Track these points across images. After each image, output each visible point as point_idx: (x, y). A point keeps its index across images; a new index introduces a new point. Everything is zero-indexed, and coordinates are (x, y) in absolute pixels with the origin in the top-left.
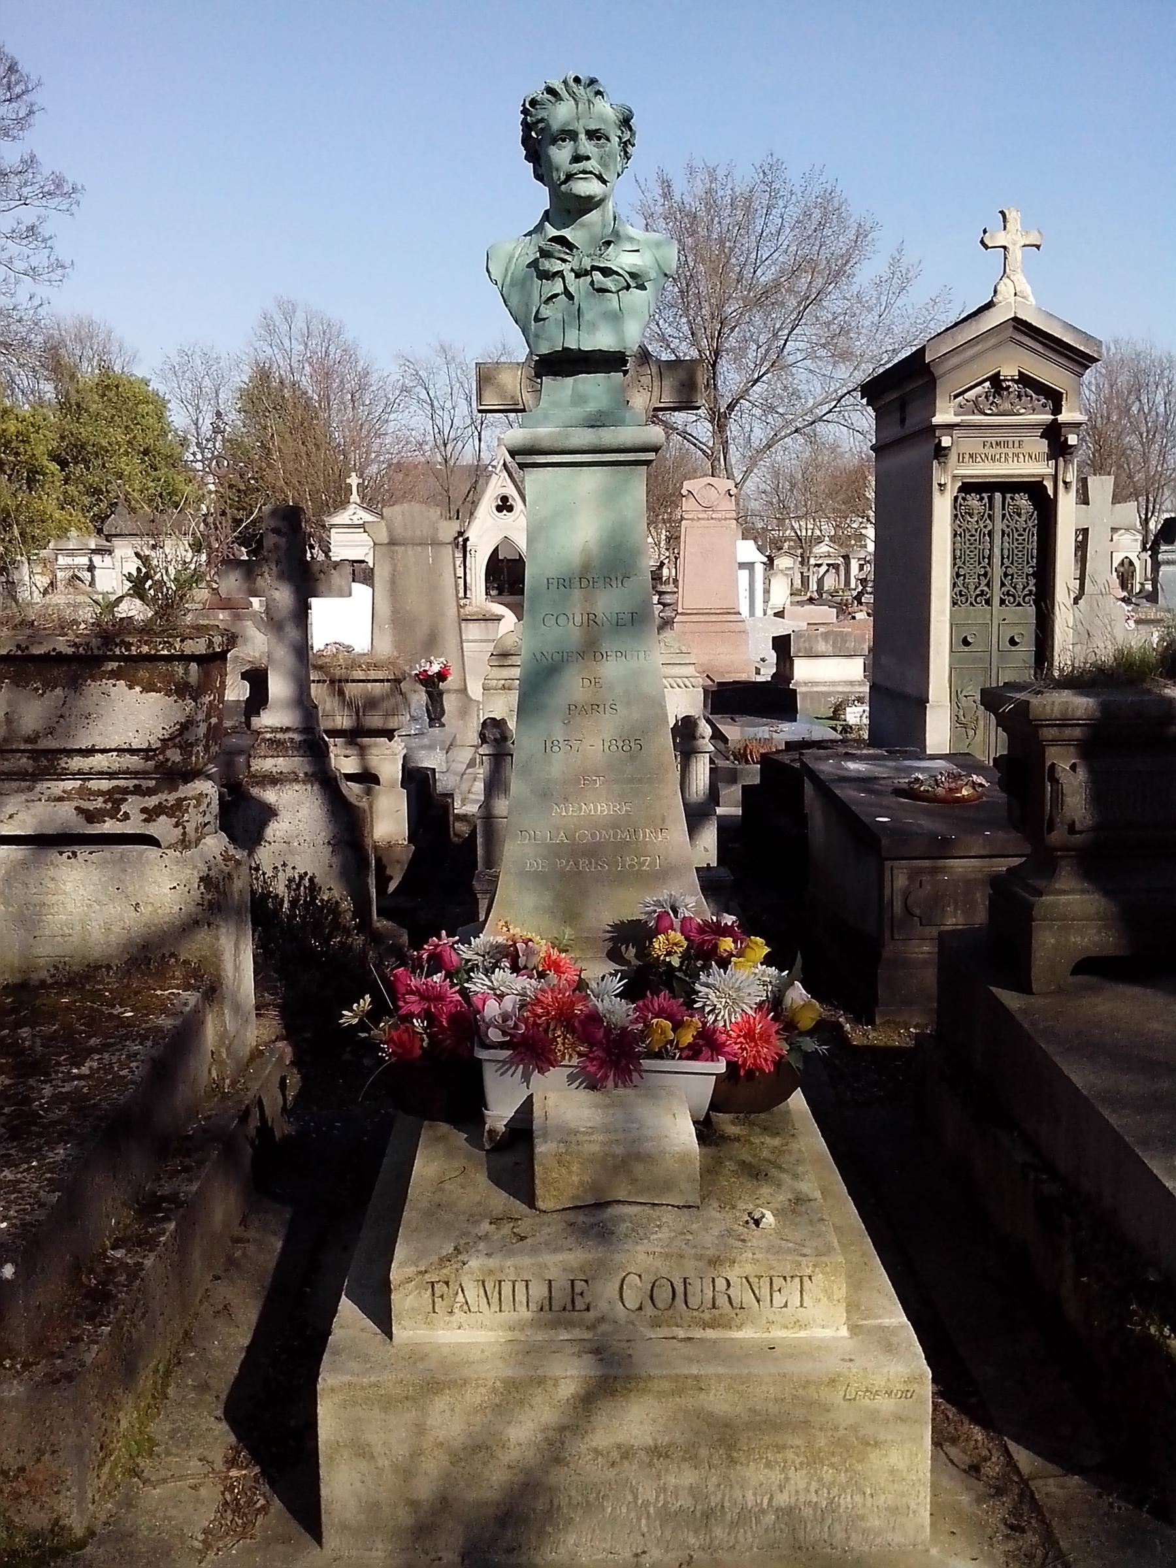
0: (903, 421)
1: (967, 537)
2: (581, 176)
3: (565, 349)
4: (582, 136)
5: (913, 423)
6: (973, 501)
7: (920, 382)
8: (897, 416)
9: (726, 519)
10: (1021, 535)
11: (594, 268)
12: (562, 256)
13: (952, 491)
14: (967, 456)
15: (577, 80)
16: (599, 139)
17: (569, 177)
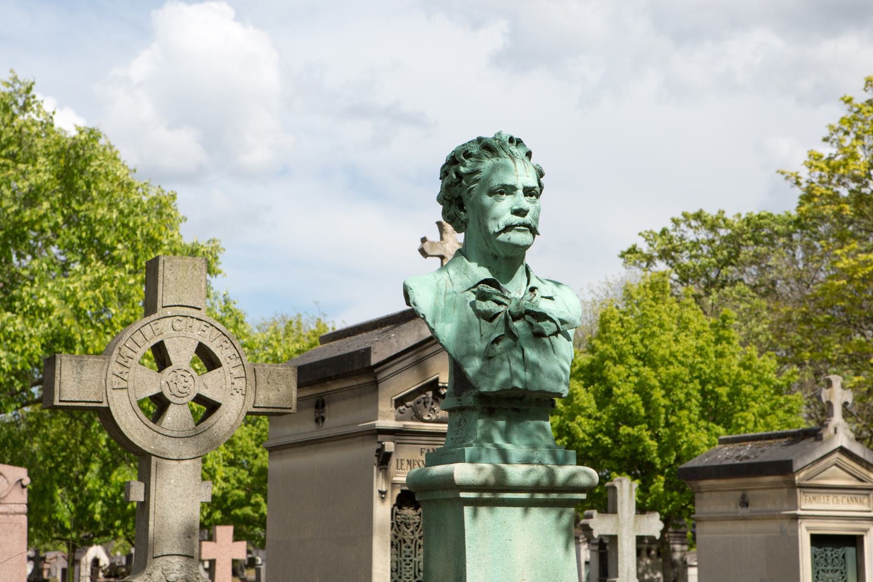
1: (403, 549)
4: (520, 192)
5: (339, 419)
7: (353, 383)
9: (15, 514)
12: (499, 298)
14: (405, 463)
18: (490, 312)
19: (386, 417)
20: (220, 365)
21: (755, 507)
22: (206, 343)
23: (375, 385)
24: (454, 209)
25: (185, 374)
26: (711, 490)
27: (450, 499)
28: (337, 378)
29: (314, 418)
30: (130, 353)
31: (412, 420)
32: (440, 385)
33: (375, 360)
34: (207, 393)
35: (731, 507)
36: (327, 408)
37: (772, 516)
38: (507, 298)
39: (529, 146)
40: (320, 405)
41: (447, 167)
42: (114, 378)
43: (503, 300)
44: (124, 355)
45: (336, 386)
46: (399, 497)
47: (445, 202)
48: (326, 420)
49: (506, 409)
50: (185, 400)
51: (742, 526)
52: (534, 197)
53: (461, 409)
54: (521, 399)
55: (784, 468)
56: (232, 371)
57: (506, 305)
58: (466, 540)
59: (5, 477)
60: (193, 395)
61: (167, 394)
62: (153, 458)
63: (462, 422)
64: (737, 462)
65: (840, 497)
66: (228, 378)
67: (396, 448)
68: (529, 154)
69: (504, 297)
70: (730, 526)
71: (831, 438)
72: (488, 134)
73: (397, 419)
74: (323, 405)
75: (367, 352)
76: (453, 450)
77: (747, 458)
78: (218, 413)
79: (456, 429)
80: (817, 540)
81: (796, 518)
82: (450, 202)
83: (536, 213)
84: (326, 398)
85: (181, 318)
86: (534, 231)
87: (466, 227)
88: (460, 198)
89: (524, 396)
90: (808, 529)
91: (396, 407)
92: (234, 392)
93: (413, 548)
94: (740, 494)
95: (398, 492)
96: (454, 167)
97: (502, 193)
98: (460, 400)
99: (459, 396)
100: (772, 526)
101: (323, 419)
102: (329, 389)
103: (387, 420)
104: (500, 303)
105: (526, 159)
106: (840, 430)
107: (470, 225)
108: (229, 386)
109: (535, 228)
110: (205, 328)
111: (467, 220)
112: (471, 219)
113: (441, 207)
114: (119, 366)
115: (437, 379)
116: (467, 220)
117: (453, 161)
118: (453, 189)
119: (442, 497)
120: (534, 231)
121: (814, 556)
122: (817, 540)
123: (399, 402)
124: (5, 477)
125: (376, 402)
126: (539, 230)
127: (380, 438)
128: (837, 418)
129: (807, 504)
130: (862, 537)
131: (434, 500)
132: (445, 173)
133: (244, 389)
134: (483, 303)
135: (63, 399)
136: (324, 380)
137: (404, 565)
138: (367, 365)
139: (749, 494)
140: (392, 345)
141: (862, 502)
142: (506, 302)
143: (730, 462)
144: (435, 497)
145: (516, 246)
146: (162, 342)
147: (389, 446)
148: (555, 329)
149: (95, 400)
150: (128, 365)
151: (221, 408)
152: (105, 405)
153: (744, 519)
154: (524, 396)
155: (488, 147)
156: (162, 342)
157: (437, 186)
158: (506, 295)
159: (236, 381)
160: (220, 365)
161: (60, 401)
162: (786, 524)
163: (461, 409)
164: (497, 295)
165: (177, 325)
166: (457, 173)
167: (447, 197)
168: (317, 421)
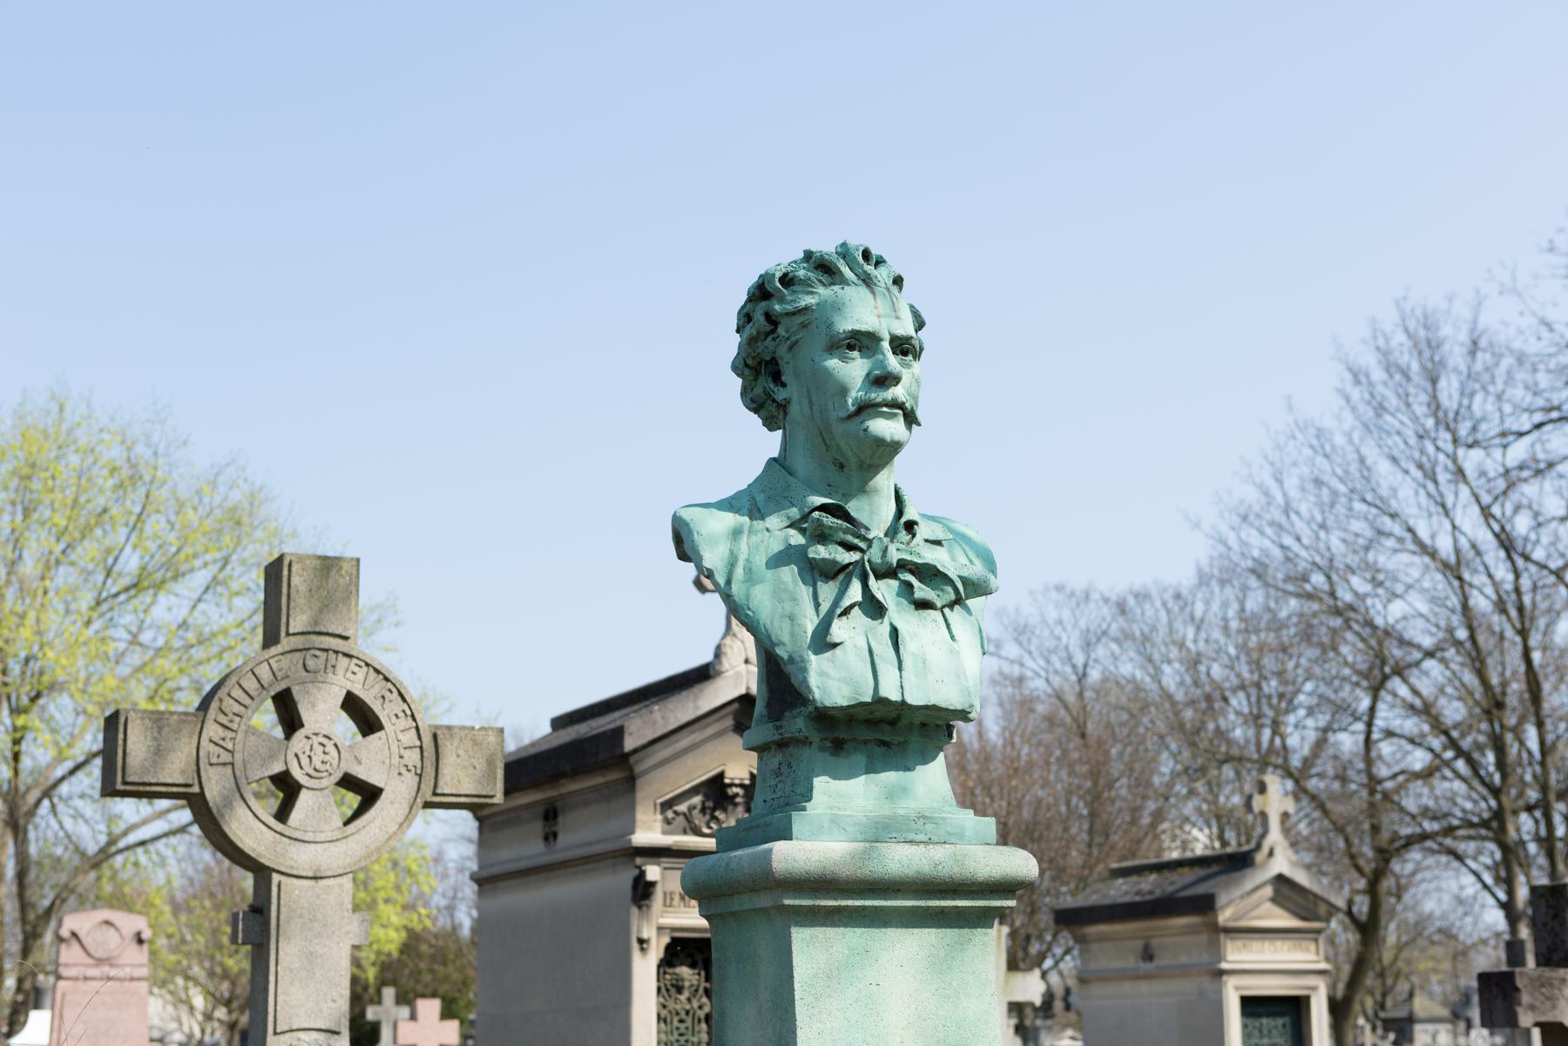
0: (550, 837)
3: (880, 701)
4: (886, 345)
5: (577, 834)
6: (685, 971)
7: (597, 780)
8: (538, 827)
10: (681, 1021)
11: (903, 565)
12: (850, 538)
13: (656, 952)
17: (866, 409)
18: (834, 562)
19: (650, 828)
20: (380, 727)
21: (1163, 960)
22: (358, 691)
23: (631, 782)
24: (765, 382)
25: (325, 741)
26: (1102, 938)
27: (764, 910)
28: (575, 773)
29: (541, 835)
30: (237, 708)
31: (685, 832)
32: (727, 781)
33: (629, 744)
34: (361, 773)
35: (1132, 962)
36: (560, 819)
37: (1184, 971)
38: (864, 539)
39: (895, 266)
40: (551, 814)
41: (749, 306)
42: (212, 748)
43: (856, 541)
44: (227, 710)
45: (573, 786)
46: (668, 948)
47: (747, 371)
48: (560, 838)
49: (866, 742)
50: (325, 783)
51: (1144, 987)
52: (910, 357)
53: (782, 745)
54: (893, 723)
55: (1205, 905)
56: (401, 736)
57: (862, 551)
58: (797, 986)
59: (117, 929)
60: (338, 776)
61: (297, 774)
62: (276, 877)
63: (784, 768)
64: (1138, 899)
65: (1279, 944)
66: (394, 748)
67: (663, 876)
68: (898, 281)
69: (859, 537)
70: (1127, 987)
71: (1264, 865)
72: (826, 246)
73: (664, 833)
74: (555, 815)
75: (618, 733)
76: (768, 819)
77: (1151, 892)
78: (379, 804)
79: (773, 782)
80: (1252, 1006)
81: (1222, 973)
82: (756, 372)
83: (914, 386)
84: (559, 805)
85: (318, 653)
86: (911, 419)
87: (786, 414)
88: (774, 362)
89: (899, 718)
90: (1237, 988)
91: (663, 812)
92: (403, 770)
93: (689, 1023)
94: (1140, 944)
95: (666, 940)
96: (764, 304)
97: (851, 347)
98: (778, 728)
99: (778, 720)
100: (1188, 986)
101: (555, 835)
102: (563, 791)
103: (649, 832)
104: (849, 547)
105: (895, 289)
106: (1278, 852)
107: (794, 409)
108: (396, 760)
109: (912, 411)
110: (356, 669)
111: (788, 401)
112: (795, 399)
113: (740, 380)
114: (220, 730)
115: (721, 776)
116: (788, 401)
117: (761, 292)
118: (760, 347)
119: (747, 906)
120: (911, 419)
121: (1245, 1026)
122: (1252, 1006)
123: (667, 805)
124: (117, 929)
125: (631, 808)
126: (920, 415)
127: (638, 861)
128: (1275, 836)
129: (1236, 955)
130: (1307, 999)
131: (734, 914)
132: (745, 317)
133: (419, 765)
134: (820, 548)
135: (130, 779)
136: (556, 777)
137: (676, 1023)
138: (618, 752)
139: (1155, 942)
140: (655, 723)
141: (1307, 950)
142: (863, 545)
143: (1127, 899)
144: (736, 908)
145: (879, 442)
146: (288, 691)
147: (653, 872)
148: (953, 597)
149: (181, 781)
150: (235, 726)
151: (384, 795)
152: (196, 789)
153: (1148, 977)
154: (899, 718)
155: (825, 268)
156: (288, 691)
157: (731, 343)
158: (863, 531)
159: (407, 754)
160: (380, 727)
161: (125, 783)
162: (1206, 983)
163: (782, 745)
164: (846, 531)
165: (311, 663)
166: (768, 317)
167: (749, 362)
168: (546, 838)
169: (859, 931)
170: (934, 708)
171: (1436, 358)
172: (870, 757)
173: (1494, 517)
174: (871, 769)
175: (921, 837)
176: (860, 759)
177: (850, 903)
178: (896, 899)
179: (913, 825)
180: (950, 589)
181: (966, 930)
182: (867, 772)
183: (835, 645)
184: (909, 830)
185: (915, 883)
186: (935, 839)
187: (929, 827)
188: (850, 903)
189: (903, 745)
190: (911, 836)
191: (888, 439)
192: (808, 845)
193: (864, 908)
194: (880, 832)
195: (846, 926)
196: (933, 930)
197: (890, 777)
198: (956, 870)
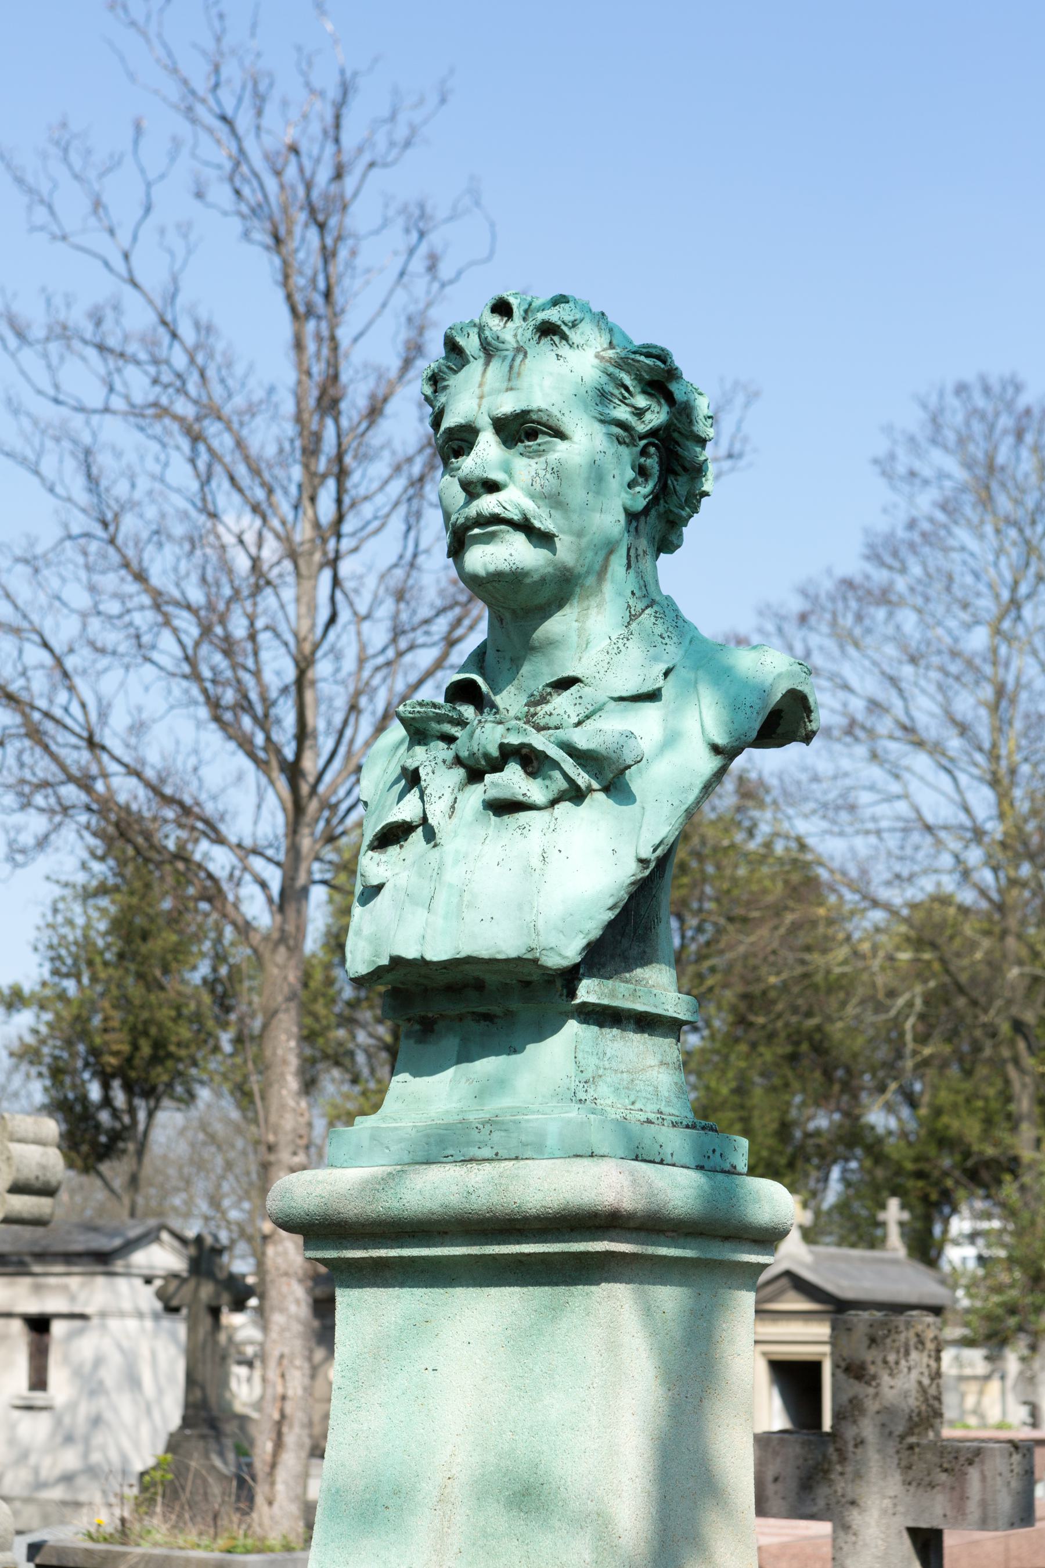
2: (476, 531)
15: (502, 308)
16: (532, 435)
49: (461, 1018)
169: (419, 1292)
170: (469, 960)
171: (415, 235)
172: (465, 1040)
173: (278, 536)
174: (465, 1057)
175: (486, 1152)
176: (451, 1043)
177: (383, 1253)
178: (442, 1244)
179: (475, 1135)
180: (557, 774)
181: (561, 1289)
182: (459, 1062)
183: (379, 888)
184: (469, 1144)
185: (488, 1220)
186: (503, 1153)
187: (497, 1136)
188: (383, 1253)
189: (509, 1014)
190: (474, 1152)
191: (482, 572)
192: (337, 1172)
193: (412, 1260)
194: (439, 1146)
195: (402, 1285)
196: (517, 1289)
197: (487, 1066)
198: (495, 1199)
